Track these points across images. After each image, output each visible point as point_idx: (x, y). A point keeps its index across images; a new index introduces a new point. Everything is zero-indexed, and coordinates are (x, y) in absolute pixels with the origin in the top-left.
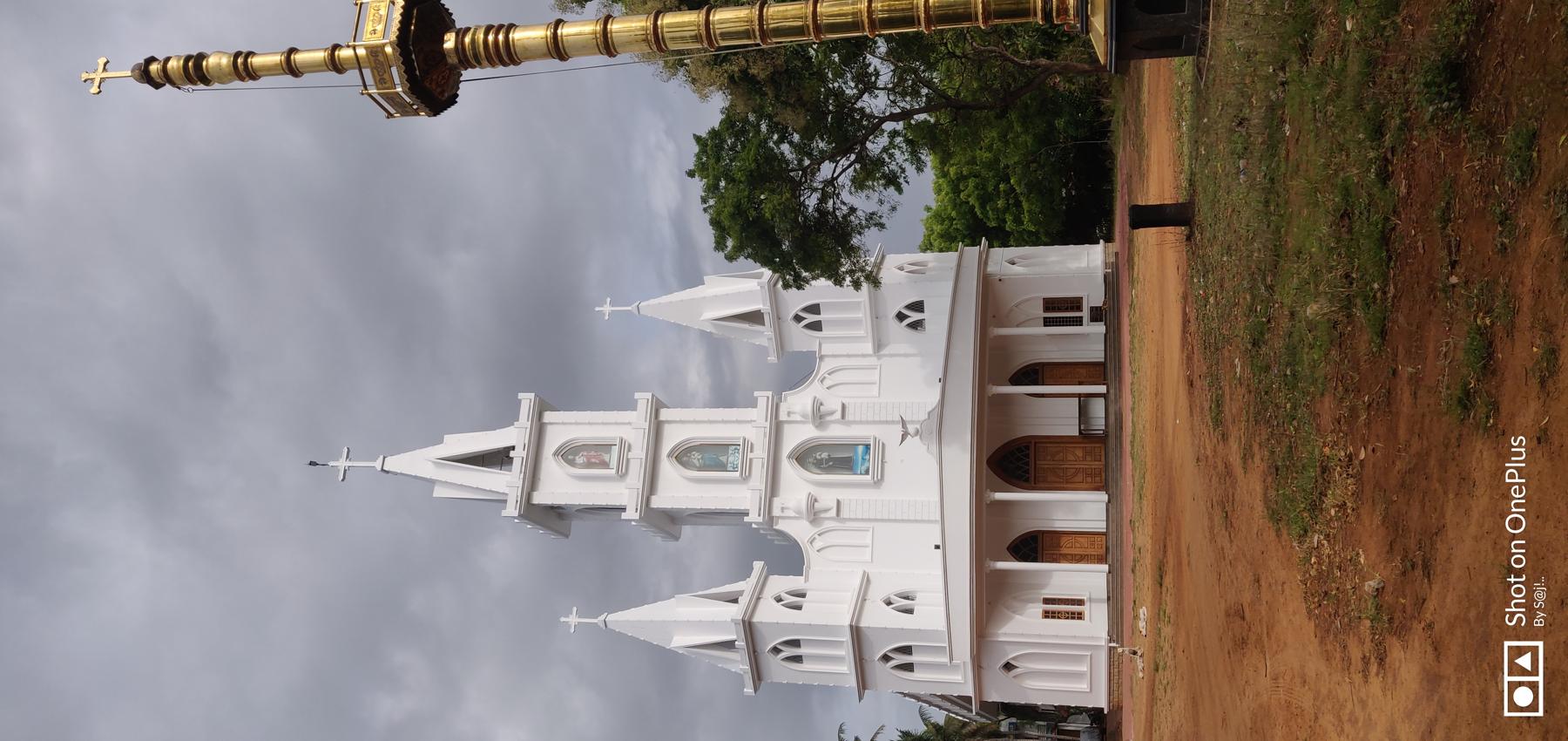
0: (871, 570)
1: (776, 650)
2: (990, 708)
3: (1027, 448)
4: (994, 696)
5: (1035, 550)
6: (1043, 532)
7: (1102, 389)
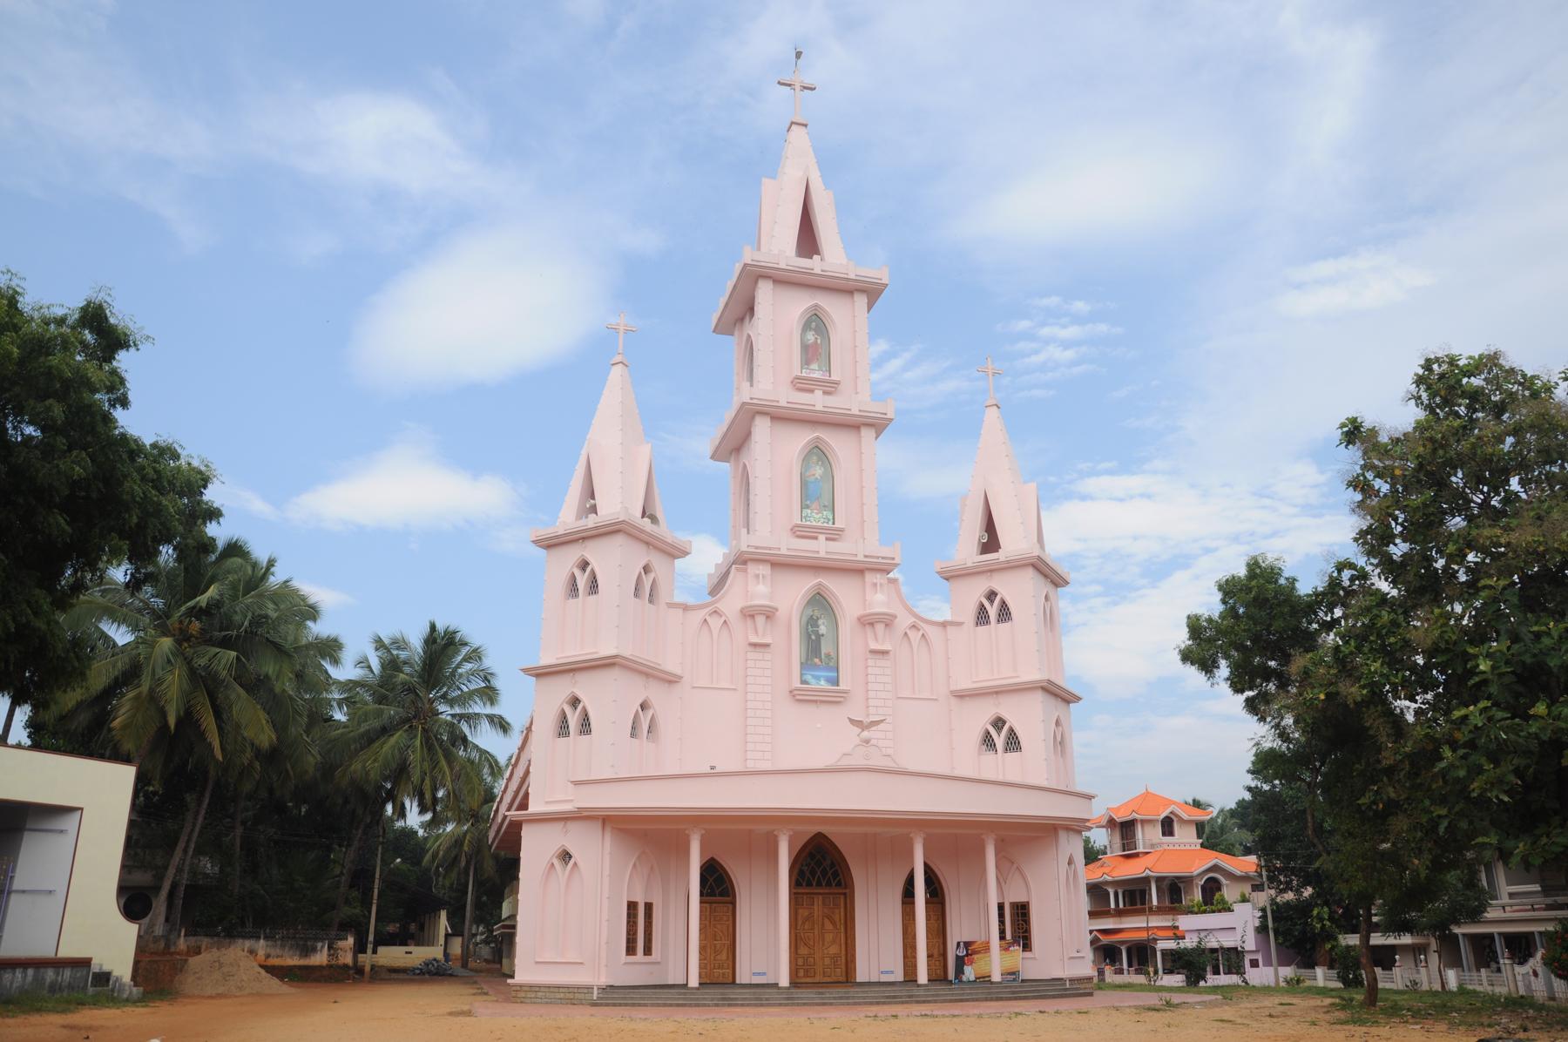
1: (584, 565)
2: (512, 837)
3: (839, 884)
4: (529, 837)
5: (712, 894)
6: (734, 903)
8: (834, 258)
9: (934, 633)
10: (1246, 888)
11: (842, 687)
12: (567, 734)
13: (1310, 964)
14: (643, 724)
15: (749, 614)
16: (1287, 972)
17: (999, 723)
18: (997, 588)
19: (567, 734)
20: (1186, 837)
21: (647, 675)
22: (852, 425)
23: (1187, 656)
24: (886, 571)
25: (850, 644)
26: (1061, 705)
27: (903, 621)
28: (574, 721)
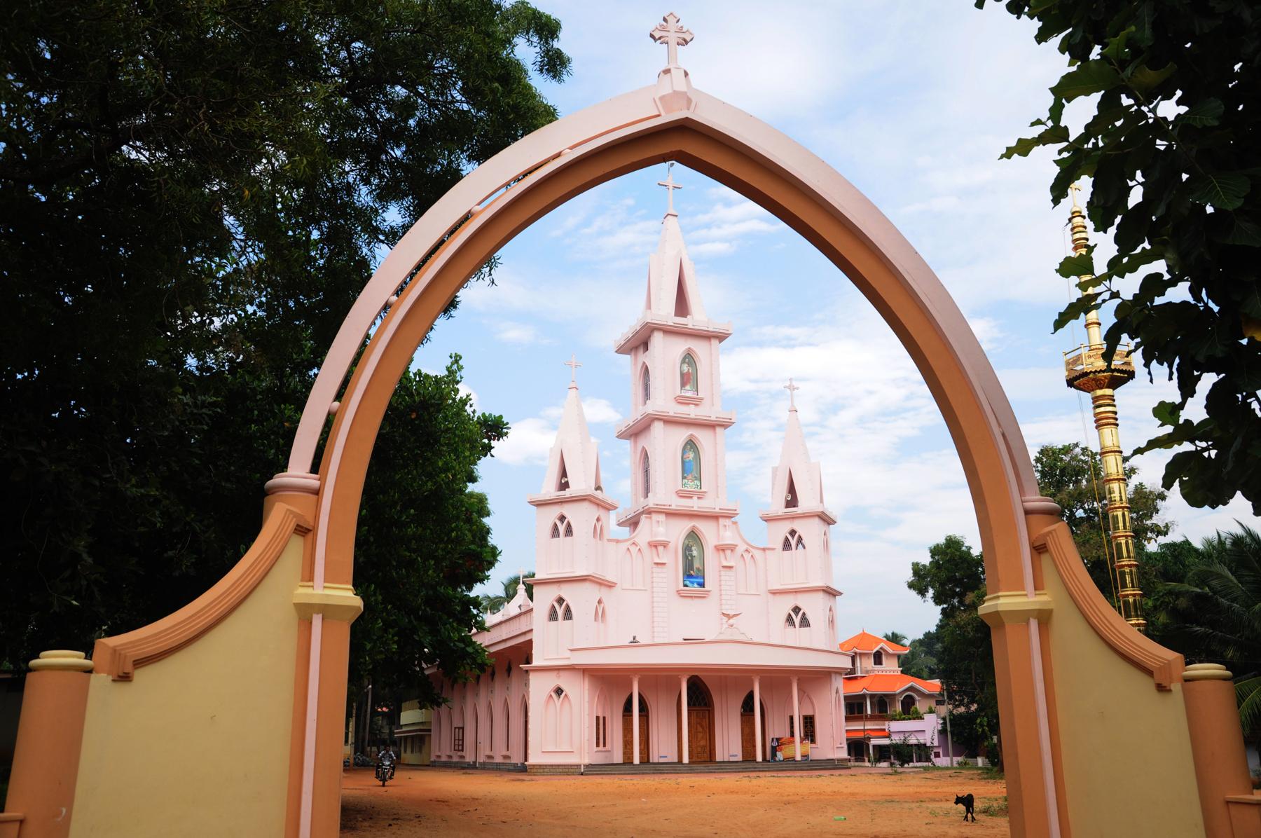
0: (616, 590)
7: (686, 760)
8: (698, 318)
9: (757, 554)
10: (933, 704)
11: (707, 588)
12: (556, 619)
13: (974, 756)
14: (600, 614)
15: (654, 545)
16: (960, 759)
17: (797, 610)
18: (796, 529)
19: (556, 619)
20: (891, 667)
21: (600, 584)
22: (711, 426)
23: (911, 586)
24: (729, 517)
25: (711, 564)
26: (832, 598)
27: (742, 548)
28: (561, 611)
